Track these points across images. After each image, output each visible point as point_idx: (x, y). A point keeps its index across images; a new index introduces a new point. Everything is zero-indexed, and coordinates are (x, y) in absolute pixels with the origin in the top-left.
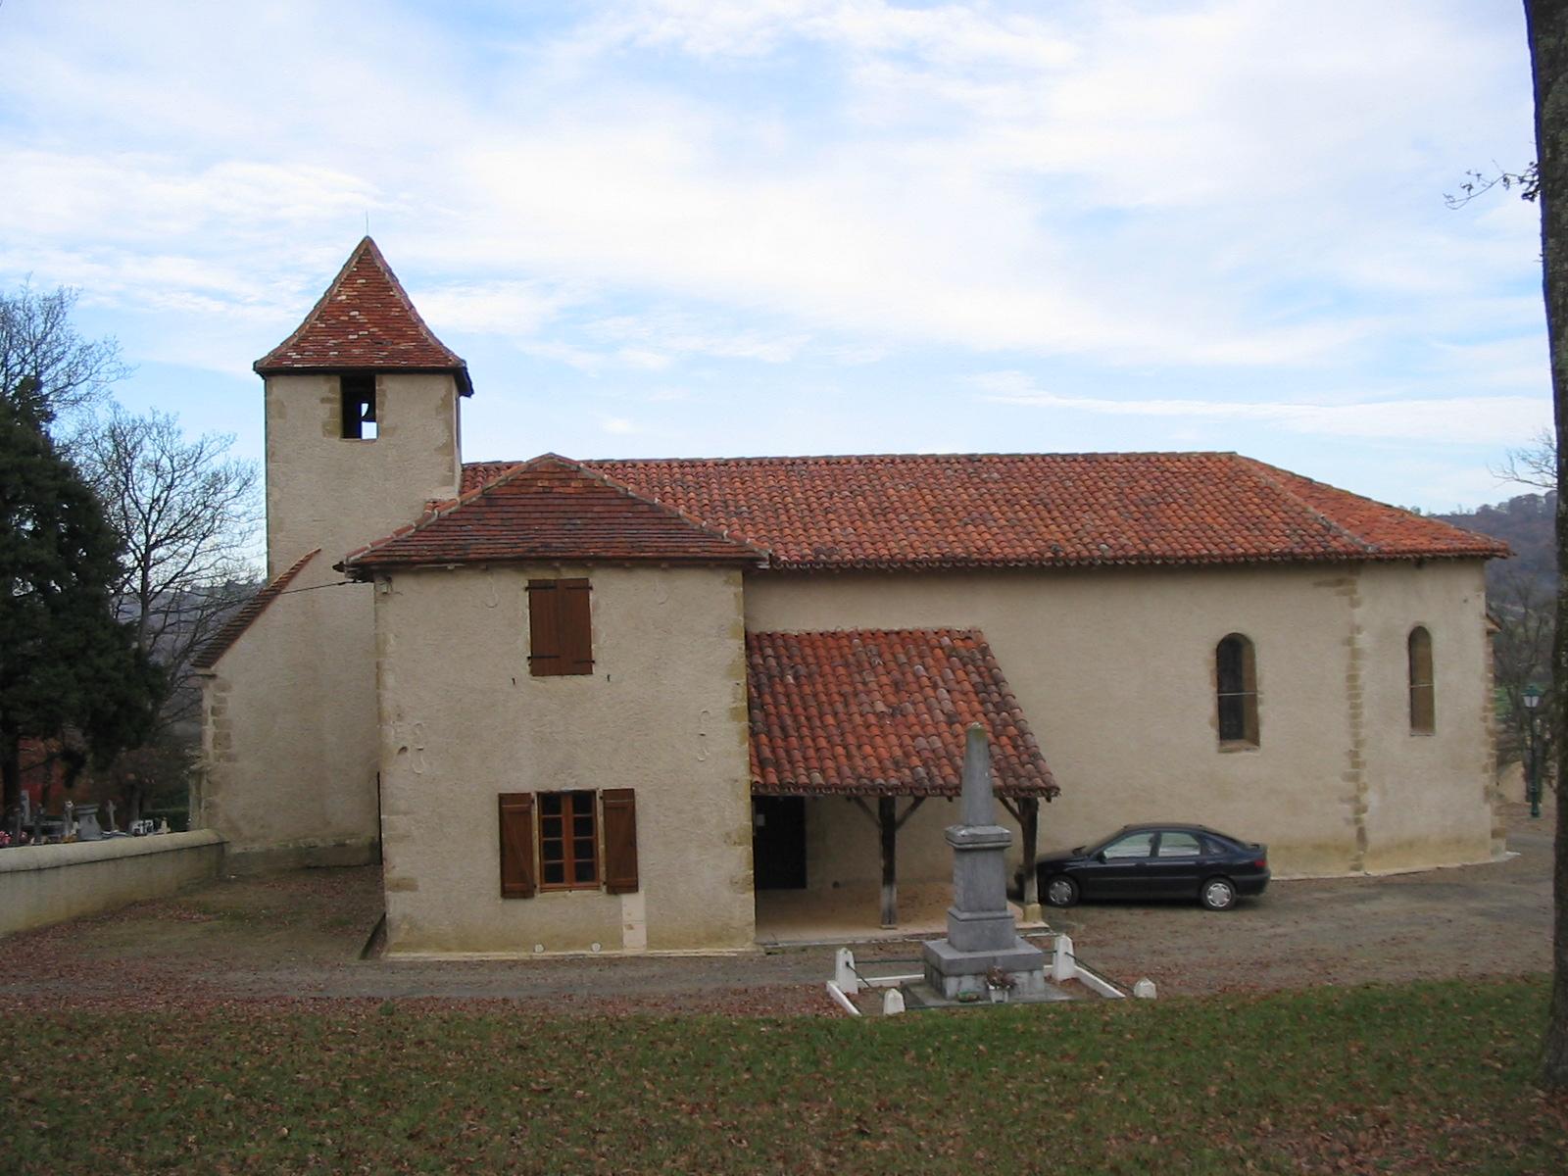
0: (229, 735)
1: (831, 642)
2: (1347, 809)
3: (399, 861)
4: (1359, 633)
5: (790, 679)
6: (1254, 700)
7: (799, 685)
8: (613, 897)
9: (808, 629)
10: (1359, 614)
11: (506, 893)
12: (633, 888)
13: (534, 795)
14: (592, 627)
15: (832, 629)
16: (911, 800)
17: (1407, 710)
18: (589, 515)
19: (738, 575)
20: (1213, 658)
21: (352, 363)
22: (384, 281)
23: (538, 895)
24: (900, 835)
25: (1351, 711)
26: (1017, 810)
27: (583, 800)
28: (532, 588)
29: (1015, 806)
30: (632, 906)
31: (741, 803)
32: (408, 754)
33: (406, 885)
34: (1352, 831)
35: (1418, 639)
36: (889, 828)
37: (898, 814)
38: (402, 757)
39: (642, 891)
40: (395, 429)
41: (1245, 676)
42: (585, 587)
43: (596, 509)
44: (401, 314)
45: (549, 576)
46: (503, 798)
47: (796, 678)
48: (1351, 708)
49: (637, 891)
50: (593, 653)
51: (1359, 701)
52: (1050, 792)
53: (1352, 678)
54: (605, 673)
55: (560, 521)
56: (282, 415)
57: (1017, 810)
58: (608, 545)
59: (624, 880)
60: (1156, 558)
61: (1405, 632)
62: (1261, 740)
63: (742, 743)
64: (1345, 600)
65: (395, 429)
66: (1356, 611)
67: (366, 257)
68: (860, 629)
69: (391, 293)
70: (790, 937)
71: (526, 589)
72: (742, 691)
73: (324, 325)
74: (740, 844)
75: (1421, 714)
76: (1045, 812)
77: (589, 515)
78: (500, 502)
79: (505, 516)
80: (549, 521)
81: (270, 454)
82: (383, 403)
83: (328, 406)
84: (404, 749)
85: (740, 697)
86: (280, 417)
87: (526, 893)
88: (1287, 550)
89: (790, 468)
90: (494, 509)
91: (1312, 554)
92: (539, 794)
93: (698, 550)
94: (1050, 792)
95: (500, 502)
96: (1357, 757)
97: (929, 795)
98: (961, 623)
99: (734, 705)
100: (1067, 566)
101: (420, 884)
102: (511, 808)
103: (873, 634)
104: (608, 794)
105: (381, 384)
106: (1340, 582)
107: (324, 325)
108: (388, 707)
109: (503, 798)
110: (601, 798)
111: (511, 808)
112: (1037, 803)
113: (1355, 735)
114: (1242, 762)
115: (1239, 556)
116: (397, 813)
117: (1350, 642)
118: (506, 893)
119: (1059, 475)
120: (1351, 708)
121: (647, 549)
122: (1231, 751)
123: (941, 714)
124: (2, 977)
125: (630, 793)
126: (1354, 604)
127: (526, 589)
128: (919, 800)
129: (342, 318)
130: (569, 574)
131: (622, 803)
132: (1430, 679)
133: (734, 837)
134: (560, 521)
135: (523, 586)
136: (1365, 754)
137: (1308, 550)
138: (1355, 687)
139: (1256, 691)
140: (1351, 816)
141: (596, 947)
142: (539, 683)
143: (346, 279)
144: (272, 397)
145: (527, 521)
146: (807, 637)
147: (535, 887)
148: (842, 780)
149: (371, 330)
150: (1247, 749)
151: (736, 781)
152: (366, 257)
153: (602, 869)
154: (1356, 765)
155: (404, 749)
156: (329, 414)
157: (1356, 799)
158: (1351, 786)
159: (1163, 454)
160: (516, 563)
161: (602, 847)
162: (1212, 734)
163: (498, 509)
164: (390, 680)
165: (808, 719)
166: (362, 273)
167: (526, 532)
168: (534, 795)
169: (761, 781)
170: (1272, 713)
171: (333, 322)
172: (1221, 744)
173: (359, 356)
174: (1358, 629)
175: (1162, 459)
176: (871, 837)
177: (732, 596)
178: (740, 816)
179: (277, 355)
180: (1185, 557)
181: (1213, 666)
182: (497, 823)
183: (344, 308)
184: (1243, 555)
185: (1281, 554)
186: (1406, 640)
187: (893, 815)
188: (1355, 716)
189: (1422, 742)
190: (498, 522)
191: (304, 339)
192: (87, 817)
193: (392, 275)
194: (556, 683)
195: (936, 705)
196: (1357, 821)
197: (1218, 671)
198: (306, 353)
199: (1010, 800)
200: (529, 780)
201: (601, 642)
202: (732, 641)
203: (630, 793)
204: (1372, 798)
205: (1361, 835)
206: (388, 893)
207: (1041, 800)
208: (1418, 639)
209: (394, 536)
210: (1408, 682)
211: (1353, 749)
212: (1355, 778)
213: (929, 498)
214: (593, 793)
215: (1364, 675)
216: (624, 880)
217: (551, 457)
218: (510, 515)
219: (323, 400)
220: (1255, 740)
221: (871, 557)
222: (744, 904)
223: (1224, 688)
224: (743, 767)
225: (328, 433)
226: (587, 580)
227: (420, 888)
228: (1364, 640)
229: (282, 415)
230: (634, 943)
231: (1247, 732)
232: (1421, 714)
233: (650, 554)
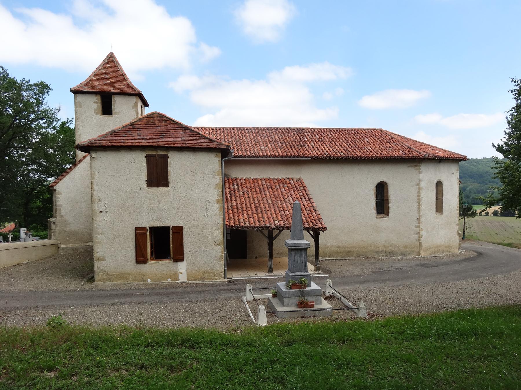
0: (61, 209)
1: (255, 181)
2: (416, 236)
3: (99, 251)
4: (421, 182)
5: (241, 193)
6: (387, 202)
7: (244, 195)
8: (175, 263)
9: (248, 177)
10: (421, 176)
11: (138, 262)
12: (182, 260)
13: (148, 228)
14: (169, 171)
15: (256, 177)
16: (278, 231)
17: (435, 206)
18: (169, 133)
19: (220, 155)
20: (375, 189)
21: (104, 90)
22: (116, 66)
23: (149, 262)
24: (274, 242)
25: (418, 206)
26: (313, 235)
27: (166, 229)
28: (148, 157)
29: (312, 233)
30: (182, 266)
31: (220, 231)
32: (102, 213)
33: (102, 259)
34: (418, 243)
35: (439, 184)
36: (271, 239)
37: (274, 236)
38: (100, 214)
39: (185, 261)
40: (119, 113)
41: (385, 195)
42: (166, 157)
43: (171, 131)
44: (122, 76)
45: (154, 153)
46: (136, 229)
47: (243, 192)
48: (418, 205)
49: (184, 261)
50: (169, 180)
51: (421, 203)
52: (324, 229)
53: (419, 196)
54: (173, 186)
55: (158, 134)
56: (81, 107)
57: (313, 235)
58: (175, 143)
59: (179, 257)
60: (358, 157)
61: (435, 182)
62: (390, 215)
63: (220, 211)
64: (417, 171)
65: (119, 113)
66: (420, 175)
67: (111, 60)
68: (265, 177)
69: (119, 70)
70: (236, 275)
71: (145, 157)
72: (220, 193)
73: (95, 79)
74: (219, 245)
75: (439, 208)
76: (322, 235)
77: (169, 133)
78: (137, 127)
79: (139, 132)
80: (154, 134)
81: (76, 119)
82: (115, 104)
83: (96, 104)
84: (101, 212)
85: (220, 195)
86: (80, 107)
87: (145, 262)
88: (399, 155)
89: (246, 130)
90: (135, 130)
91: (408, 157)
92: (150, 228)
93: (206, 145)
94: (324, 229)
95: (137, 127)
96: (420, 220)
97: (284, 230)
98: (296, 176)
99: (217, 198)
100: (330, 159)
101: (107, 258)
102: (140, 232)
103: (269, 179)
104: (174, 228)
105: (114, 98)
106: (416, 166)
107: (95, 79)
108: (95, 197)
109: (136, 229)
110: (171, 229)
111: (140, 232)
112: (320, 233)
113: (419, 213)
114: (384, 221)
115: (384, 157)
116: (98, 234)
117: (418, 185)
118: (138, 262)
119: (328, 134)
120: (418, 205)
121: (188, 144)
122: (380, 218)
123: (289, 204)
124: (520, 232)
125: (181, 227)
126: (420, 173)
127: (145, 157)
128: (280, 232)
129: (102, 77)
130: (160, 152)
131: (179, 231)
132: (442, 197)
133: (217, 243)
134: (158, 134)
135: (144, 156)
136: (422, 219)
137: (406, 155)
138: (419, 199)
139: (388, 199)
140: (417, 239)
141: (169, 280)
142: (151, 190)
143: (104, 65)
144: (77, 101)
145: (146, 134)
146: (248, 180)
147: (148, 259)
148: (255, 225)
149: (111, 81)
150: (385, 217)
151: (218, 224)
152: (111, 60)
153: (172, 253)
154: (419, 223)
155: (101, 212)
156: (96, 107)
157: (419, 233)
158: (418, 229)
159: (360, 129)
160: (142, 148)
161: (171, 246)
162: (375, 212)
163: (137, 129)
164: (96, 188)
165: (246, 205)
166: (109, 63)
167: (146, 138)
168: (148, 228)
169: (228, 224)
170: (393, 206)
171: (99, 78)
172: (377, 216)
173: (106, 88)
174: (421, 181)
175: (359, 130)
176: (266, 242)
177: (218, 161)
178: (219, 235)
179: (79, 87)
180: (368, 157)
181: (375, 191)
182: (135, 237)
183: (102, 73)
184: (386, 156)
185: (398, 156)
186: (435, 185)
187: (272, 236)
188: (419, 208)
189: (439, 216)
190: (136, 134)
191: (88, 82)
192: (28, 236)
193: (119, 64)
194: (155, 190)
195: (288, 201)
196: (419, 240)
197: (377, 193)
198: (89, 87)
199: (311, 231)
200: (146, 223)
201: (172, 176)
202: (217, 176)
203: (181, 227)
204: (423, 233)
205: (420, 245)
206: (95, 262)
207: (321, 232)
208: (439, 184)
209: (98, 137)
210: (435, 198)
211: (418, 218)
212: (419, 227)
213: (288, 139)
214: (168, 227)
215: (422, 195)
216: (179, 257)
217: (156, 113)
218: (141, 132)
219: (95, 102)
220: (388, 214)
221: (268, 155)
222: (220, 266)
223: (378, 198)
224: (72, 173)
225: (96, 113)
226: (167, 154)
227: (106, 260)
228: (423, 184)
229: (81, 107)
230: (182, 278)
231: (385, 212)
232: (439, 208)
233: (189, 146)
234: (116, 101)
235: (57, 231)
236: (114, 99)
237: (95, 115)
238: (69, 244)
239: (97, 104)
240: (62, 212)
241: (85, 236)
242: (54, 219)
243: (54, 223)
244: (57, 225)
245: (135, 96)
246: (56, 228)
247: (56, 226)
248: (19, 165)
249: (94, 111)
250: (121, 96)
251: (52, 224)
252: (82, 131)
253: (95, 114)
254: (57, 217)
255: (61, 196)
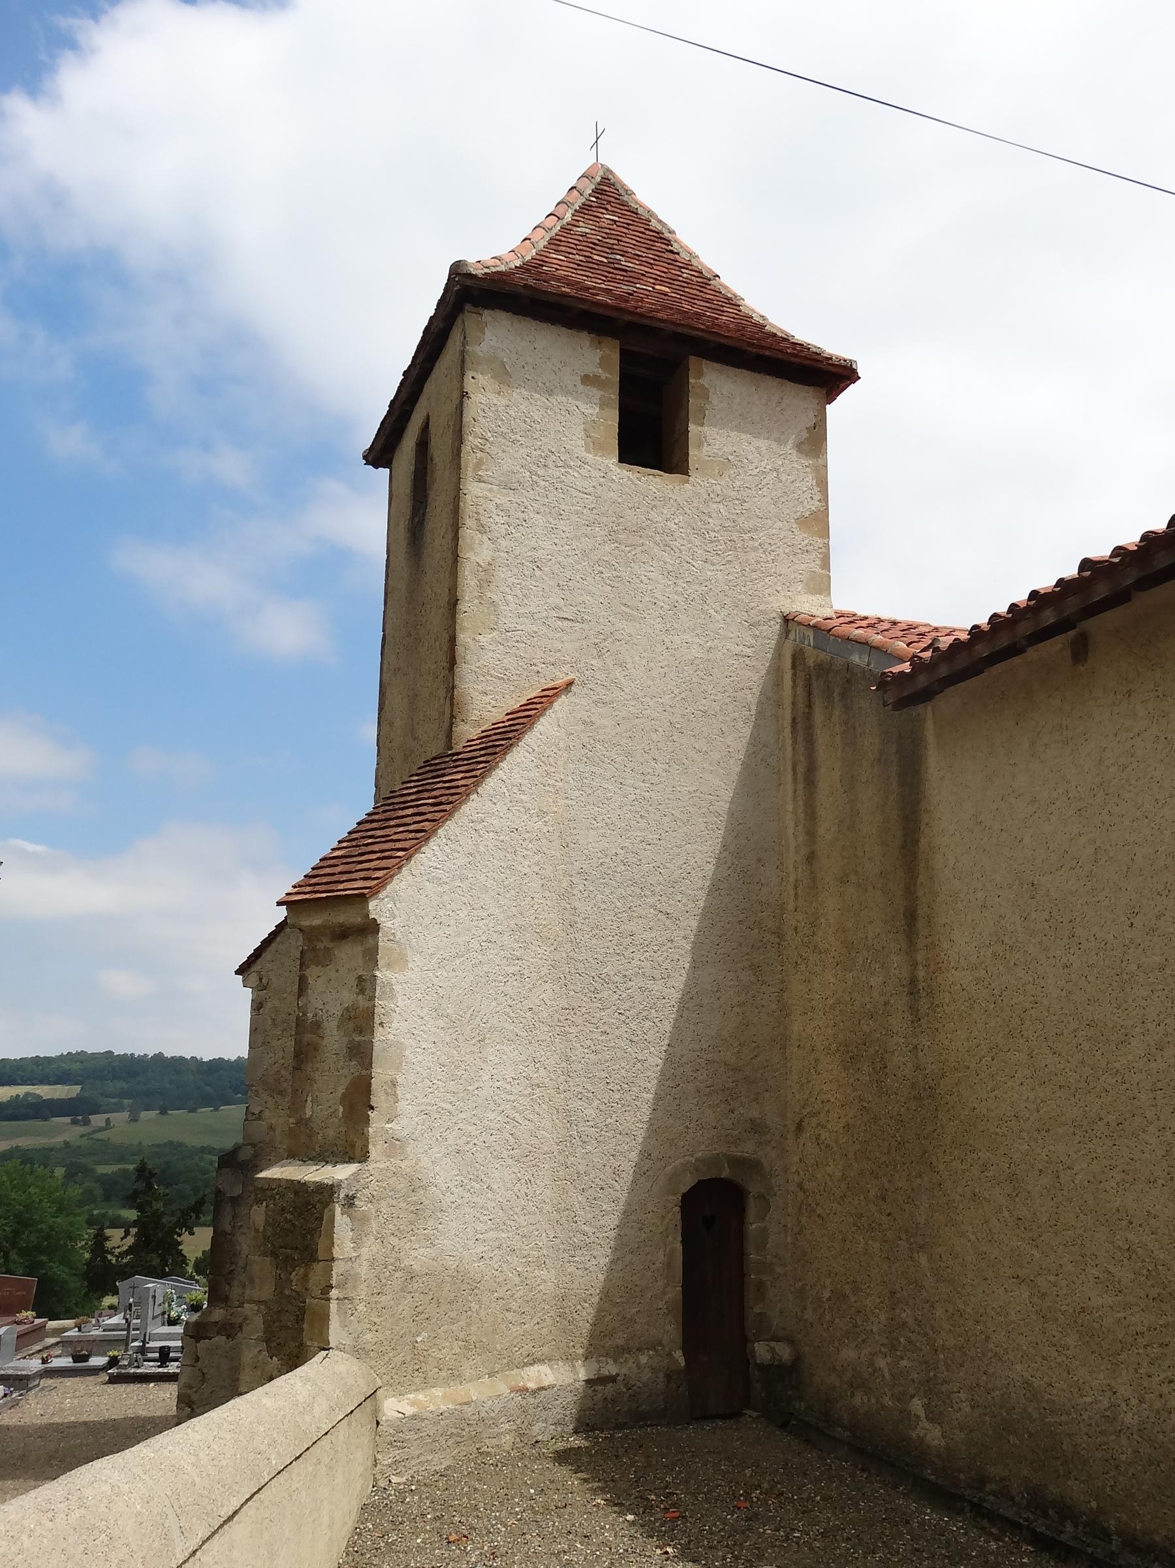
0: (394, 1084)
105: (700, 375)
225: (597, 447)
234: (714, 399)
235: (363, 1270)
236: (701, 381)
237: (585, 454)
238: (426, 1383)
239: (602, 393)
240: (402, 1106)
241: (509, 1316)
242: (352, 1168)
243: (352, 1205)
244: (364, 1219)
245: (812, 389)
246: (357, 1242)
247: (360, 1223)
248: (903, 1363)
249: (579, 432)
250: (731, 370)
251: (338, 1209)
252: (503, 543)
253: (588, 451)
254: (374, 1152)
255: (401, 978)
